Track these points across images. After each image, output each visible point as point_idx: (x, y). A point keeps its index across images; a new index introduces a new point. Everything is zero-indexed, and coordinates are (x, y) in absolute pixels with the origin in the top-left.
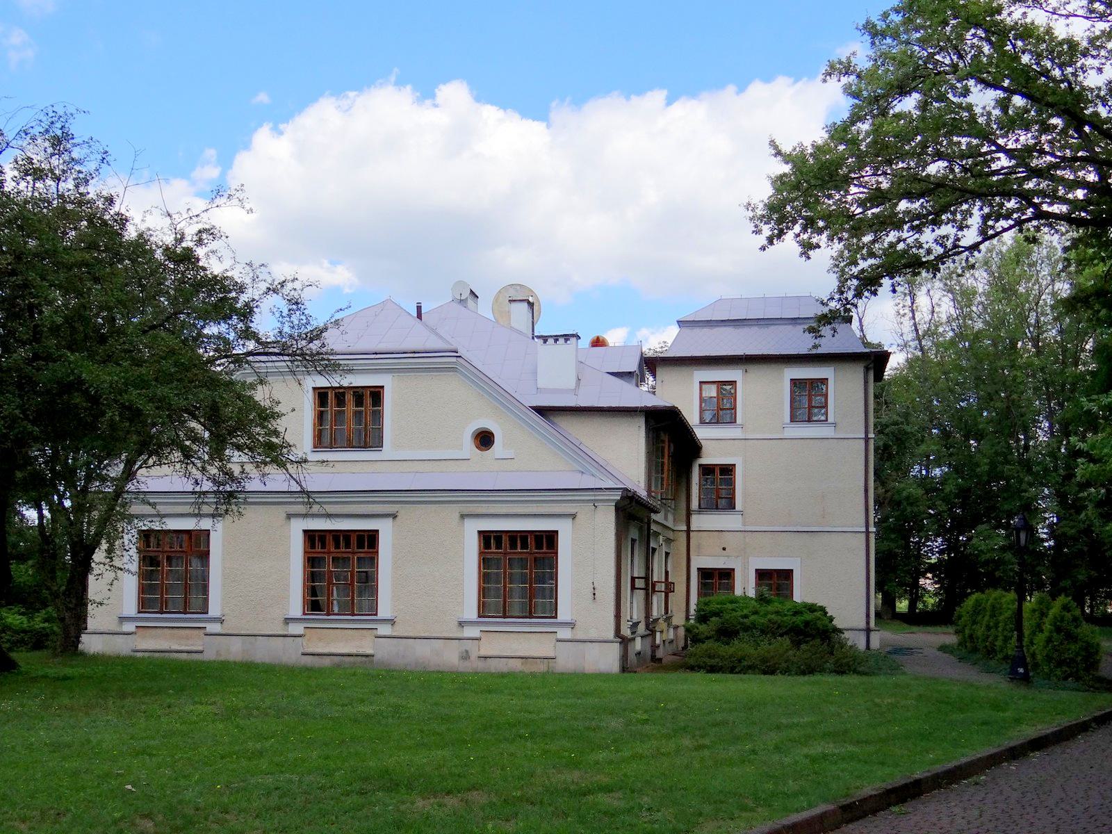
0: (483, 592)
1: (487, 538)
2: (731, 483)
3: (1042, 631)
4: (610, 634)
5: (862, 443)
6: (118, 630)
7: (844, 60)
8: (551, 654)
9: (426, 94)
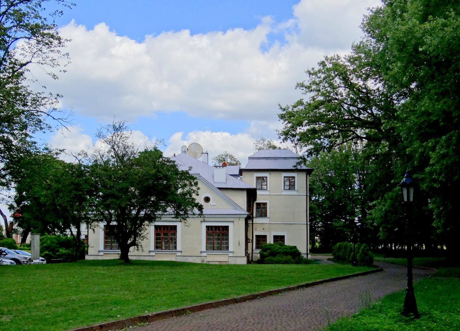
0: (105, 242)
1: (208, 227)
2: (266, 208)
3: (359, 253)
4: (244, 255)
5: (306, 196)
6: (98, 254)
7: (301, 83)
8: (227, 261)
9: (90, 27)
